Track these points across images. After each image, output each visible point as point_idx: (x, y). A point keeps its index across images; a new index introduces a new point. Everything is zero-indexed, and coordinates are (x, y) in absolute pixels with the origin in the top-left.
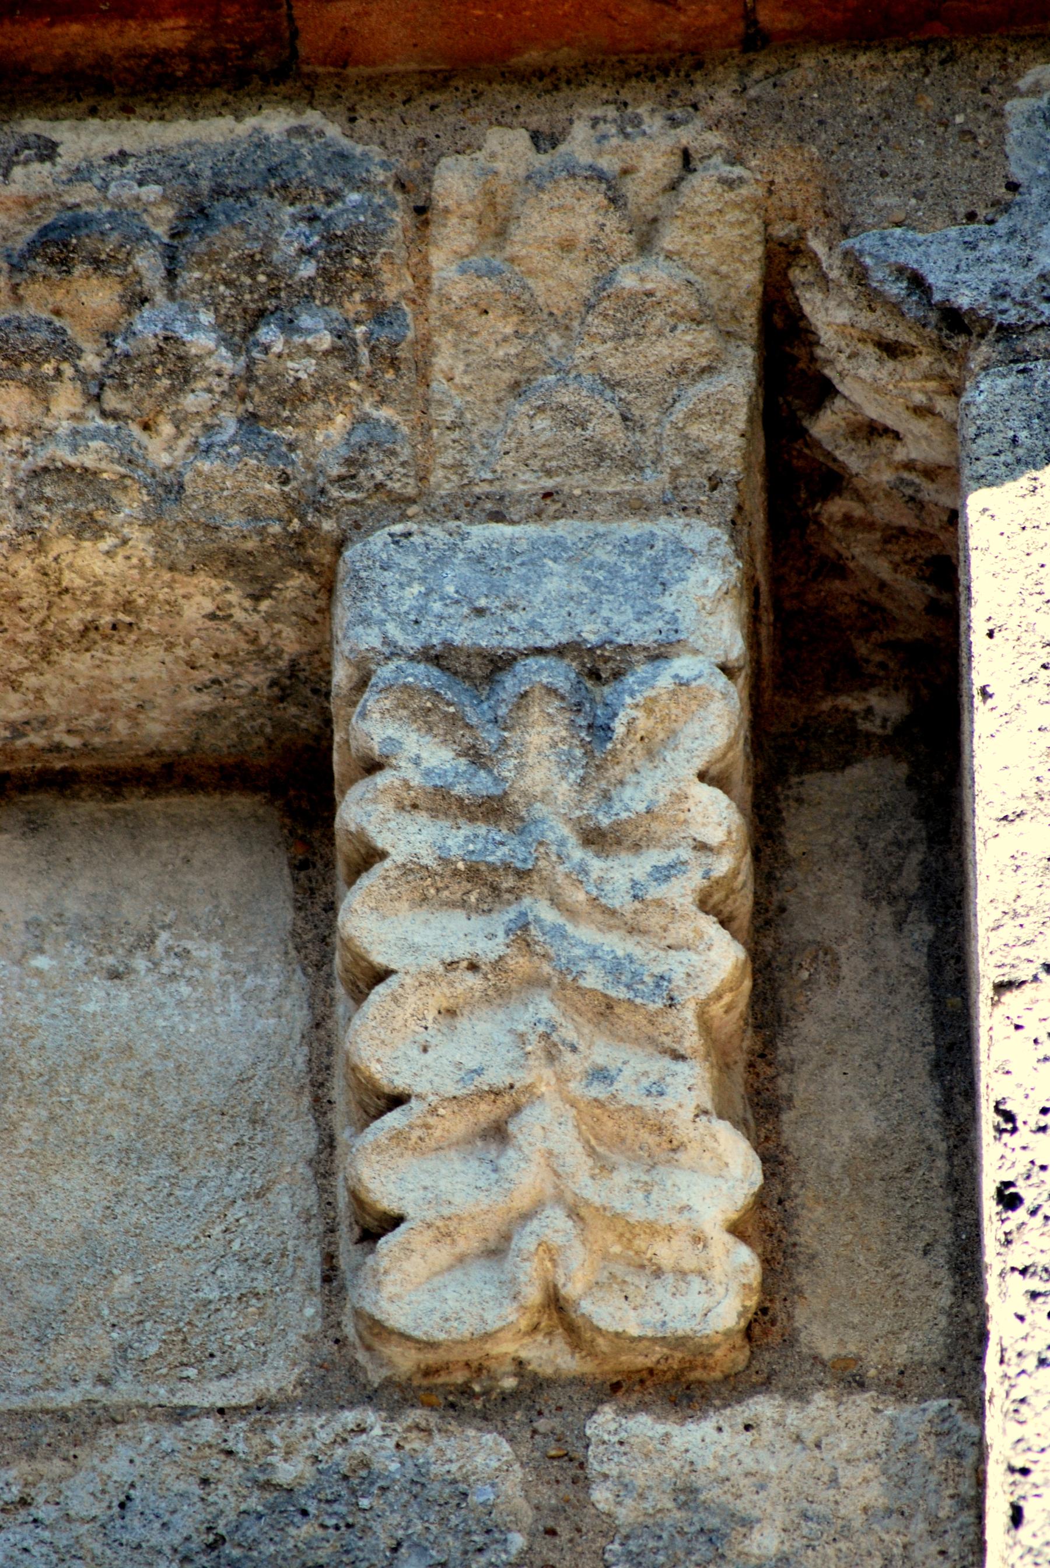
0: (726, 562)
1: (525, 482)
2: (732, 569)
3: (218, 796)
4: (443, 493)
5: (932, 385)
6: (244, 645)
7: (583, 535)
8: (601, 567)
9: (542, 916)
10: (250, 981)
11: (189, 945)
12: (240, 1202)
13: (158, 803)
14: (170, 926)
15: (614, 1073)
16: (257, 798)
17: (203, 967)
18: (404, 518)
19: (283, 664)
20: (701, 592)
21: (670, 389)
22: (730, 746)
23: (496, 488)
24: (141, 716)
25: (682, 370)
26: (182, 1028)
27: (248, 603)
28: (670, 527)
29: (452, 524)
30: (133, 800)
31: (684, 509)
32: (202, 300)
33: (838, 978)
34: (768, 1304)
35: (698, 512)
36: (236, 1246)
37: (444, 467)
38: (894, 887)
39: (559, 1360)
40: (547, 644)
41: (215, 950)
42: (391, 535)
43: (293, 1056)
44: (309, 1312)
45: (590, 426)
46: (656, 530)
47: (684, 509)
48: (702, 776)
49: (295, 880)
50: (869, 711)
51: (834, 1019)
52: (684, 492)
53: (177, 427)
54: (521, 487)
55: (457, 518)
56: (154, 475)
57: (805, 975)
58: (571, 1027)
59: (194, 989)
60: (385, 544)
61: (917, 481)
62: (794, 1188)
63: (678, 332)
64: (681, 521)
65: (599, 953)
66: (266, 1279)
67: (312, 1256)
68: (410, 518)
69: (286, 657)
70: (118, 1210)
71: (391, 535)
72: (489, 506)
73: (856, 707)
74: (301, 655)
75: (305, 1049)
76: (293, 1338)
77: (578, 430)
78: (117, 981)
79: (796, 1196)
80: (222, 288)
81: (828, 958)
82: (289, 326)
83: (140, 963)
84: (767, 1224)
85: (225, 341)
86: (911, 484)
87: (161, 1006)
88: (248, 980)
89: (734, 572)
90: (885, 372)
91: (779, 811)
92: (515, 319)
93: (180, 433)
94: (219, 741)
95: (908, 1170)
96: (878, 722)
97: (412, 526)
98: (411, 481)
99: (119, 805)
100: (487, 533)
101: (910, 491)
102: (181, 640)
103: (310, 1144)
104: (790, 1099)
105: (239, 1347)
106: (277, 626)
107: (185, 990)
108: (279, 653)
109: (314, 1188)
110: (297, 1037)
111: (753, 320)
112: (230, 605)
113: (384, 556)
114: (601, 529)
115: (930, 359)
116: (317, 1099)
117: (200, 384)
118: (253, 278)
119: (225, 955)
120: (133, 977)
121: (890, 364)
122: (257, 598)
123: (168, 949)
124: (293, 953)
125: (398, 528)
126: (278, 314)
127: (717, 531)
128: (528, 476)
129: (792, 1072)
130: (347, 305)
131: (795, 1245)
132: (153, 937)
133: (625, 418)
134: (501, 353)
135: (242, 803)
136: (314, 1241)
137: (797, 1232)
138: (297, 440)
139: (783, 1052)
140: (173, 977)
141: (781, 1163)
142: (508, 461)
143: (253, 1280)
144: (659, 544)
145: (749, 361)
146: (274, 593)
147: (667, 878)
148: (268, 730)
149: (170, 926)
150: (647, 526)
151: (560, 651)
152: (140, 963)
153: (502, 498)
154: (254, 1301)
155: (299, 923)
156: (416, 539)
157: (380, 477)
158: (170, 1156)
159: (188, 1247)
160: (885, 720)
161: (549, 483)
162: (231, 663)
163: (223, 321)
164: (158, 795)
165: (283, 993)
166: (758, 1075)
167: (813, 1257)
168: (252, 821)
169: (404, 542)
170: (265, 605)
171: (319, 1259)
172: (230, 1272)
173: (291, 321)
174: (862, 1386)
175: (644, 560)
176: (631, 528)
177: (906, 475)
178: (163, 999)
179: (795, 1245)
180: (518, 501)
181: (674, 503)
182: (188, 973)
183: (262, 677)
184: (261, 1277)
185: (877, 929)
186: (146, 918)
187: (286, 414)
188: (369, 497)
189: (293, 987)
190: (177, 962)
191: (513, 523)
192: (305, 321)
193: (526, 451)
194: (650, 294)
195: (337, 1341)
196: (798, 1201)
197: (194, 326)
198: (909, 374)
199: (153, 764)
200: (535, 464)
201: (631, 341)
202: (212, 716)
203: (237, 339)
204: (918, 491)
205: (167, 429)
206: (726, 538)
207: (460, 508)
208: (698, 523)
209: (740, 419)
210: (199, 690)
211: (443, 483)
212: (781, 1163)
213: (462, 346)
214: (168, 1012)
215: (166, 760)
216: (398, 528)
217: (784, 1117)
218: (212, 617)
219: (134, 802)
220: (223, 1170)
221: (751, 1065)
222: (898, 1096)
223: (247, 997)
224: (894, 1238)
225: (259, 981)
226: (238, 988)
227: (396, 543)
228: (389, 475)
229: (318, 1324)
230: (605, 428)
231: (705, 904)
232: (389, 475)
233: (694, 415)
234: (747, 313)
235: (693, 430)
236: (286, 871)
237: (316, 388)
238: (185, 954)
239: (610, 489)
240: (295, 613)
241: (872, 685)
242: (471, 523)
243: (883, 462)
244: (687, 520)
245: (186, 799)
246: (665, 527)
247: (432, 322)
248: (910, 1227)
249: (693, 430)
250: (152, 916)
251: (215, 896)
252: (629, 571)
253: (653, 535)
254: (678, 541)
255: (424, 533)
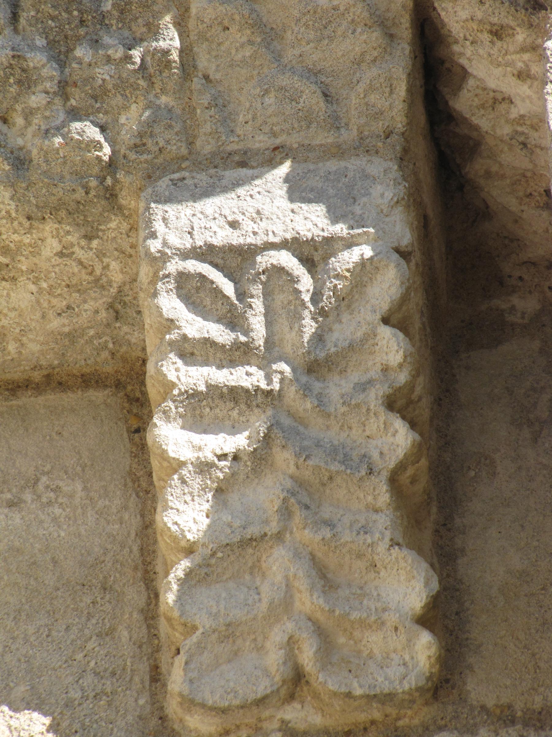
0: (396, 183)
1: (260, 142)
2: (401, 187)
3: (80, 393)
4: (206, 152)
5: (526, 56)
6: (85, 277)
7: (300, 171)
8: (312, 190)
9: (282, 421)
10: (100, 504)
11: (61, 484)
12: (94, 638)
13: (41, 399)
14: (48, 473)
15: (336, 522)
16: (106, 392)
17: (71, 496)
18: (180, 169)
19: (113, 291)
20: (380, 201)
21: (354, 73)
22: (404, 299)
23: (241, 146)
24: (24, 339)
25: (358, 62)
26: (55, 535)
27: (83, 242)
28: (358, 162)
29: (212, 171)
30: (24, 399)
31: (367, 151)
32: (38, 30)
33: (494, 474)
34: (449, 677)
35: (377, 152)
36: (92, 664)
37: (205, 134)
38: (531, 416)
39: (309, 719)
40: (277, 240)
41: (79, 486)
42: (171, 180)
43: (130, 548)
44: (141, 702)
45: (302, 100)
46: (350, 166)
47: (367, 151)
48: (386, 321)
49: (131, 440)
50: (513, 308)
51: (492, 500)
52: (368, 141)
53: (26, 119)
54: (257, 145)
55: (216, 167)
56: (12, 153)
57: (472, 473)
58: (305, 493)
59: (64, 510)
60: (167, 186)
61: (526, 131)
62: (467, 604)
63: (357, 33)
64: (365, 159)
65: (322, 443)
66: (112, 684)
67: (144, 667)
68: (184, 169)
69: (115, 285)
70: (13, 647)
71: (171, 180)
72: (237, 158)
73: (504, 306)
74: (124, 284)
75: (139, 541)
76: (130, 718)
77: (294, 103)
78: (14, 509)
79: (468, 609)
80: (50, 22)
81: (488, 461)
82: (96, 43)
83: (28, 496)
84: (444, 615)
85: (51, 58)
86: (523, 133)
87: (42, 522)
88: (100, 503)
89: (402, 190)
90: (496, 49)
91: (454, 376)
92: (249, 32)
93: (28, 123)
94: (81, 359)
95: (543, 589)
96: (519, 315)
97: (186, 174)
98: (184, 145)
99: (14, 402)
100: (235, 175)
101: (522, 139)
102: (42, 275)
103: (141, 601)
104: (463, 550)
105: (95, 726)
106: (106, 260)
107: (57, 511)
108: (110, 283)
109: (144, 627)
110: (133, 535)
111: (408, 25)
112: (72, 245)
113: (167, 193)
114: (312, 167)
115: (524, 36)
116: (146, 572)
117: (40, 88)
118: (69, 12)
119: (85, 489)
120: (22, 505)
121: (499, 44)
122: (89, 238)
123: (47, 487)
124: (130, 484)
125: (176, 176)
126: (88, 37)
127: (390, 164)
128: (261, 137)
129: (464, 533)
130: (134, 28)
131: (467, 639)
132: (37, 481)
133: (325, 95)
134: (240, 56)
135: (98, 396)
136: (145, 658)
137: (469, 632)
138: (106, 123)
139: (458, 521)
140: (50, 503)
141: (458, 590)
142: (249, 127)
143: (103, 685)
144: (351, 174)
145: (407, 52)
146: (100, 234)
147: (364, 390)
148: (111, 345)
149: (48, 473)
150: (343, 164)
151: (284, 245)
152: (28, 496)
153: (245, 153)
154: (104, 697)
155: (134, 466)
156: (188, 182)
157: (162, 144)
158: (48, 612)
159: (60, 667)
160: (523, 313)
161: (278, 141)
162: (79, 291)
163: (51, 44)
164: (40, 394)
165: (125, 508)
166: (441, 537)
167: (480, 646)
168: (102, 406)
169: (180, 184)
170: (95, 243)
171: (148, 669)
172: (88, 680)
173: (97, 41)
174: (513, 722)
175: (340, 185)
176: (333, 165)
177: (519, 129)
178: (43, 517)
179: (467, 639)
180: (257, 154)
181: (363, 147)
182: (60, 500)
183: (101, 302)
184: (109, 683)
185: (520, 442)
186: (33, 469)
187: (98, 105)
188: (156, 157)
189: (131, 505)
190: (52, 495)
191: (253, 168)
192: (107, 40)
193: (260, 121)
194: (335, 8)
195: (161, 718)
196: (469, 612)
197: (33, 48)
198: (511, 49)
199: (37, 376)
200: (266, 129)
201: (326, 41)
202: (72, 337)
203: (62, 57)
204: (528, 138)
205: (20, 121)
206: (396, 167)
207: (217, 161)
208: (376, 160)
209: (402, 90)
210: (59, 314)
211: (205, 146)
212: (458, 590)
213: (214, 53)
214: (46, 525)
215: (45, 372)
216: (176, 176)
217: (459, 561)
218: (61, 254)
219: (26, 399)
220: (84, 619)
221: (437, 531)
222: (535, 543)
223: (99, 513)
224: (533, 631)
225: (107, 503)
226: (93, 508)
227: (175, 184)
228: (168, 142)
229: (148, 708)
230: (310, 97)
231: (390, 404)
232: (168, 142)
233: (371, 88)
234: (402, 21)
235: (373, 98)
236: (125, 435)
237: (115, 86)
238: (57, 490)
239: (318, 142)
240: (116, 249)
241: (514, 292)
242: (225, 170)
243: (503, 121)
244: (369, 158)
245: (58, 395)
246: (354, 164)
247: (192, 37)
248: (544, 624)
249: (373, 98)
250: (36, 467)
251: (78, 453)
252: (331, 192)
253: (346, 168)
254: (363, 170)
255: (193, 178)
